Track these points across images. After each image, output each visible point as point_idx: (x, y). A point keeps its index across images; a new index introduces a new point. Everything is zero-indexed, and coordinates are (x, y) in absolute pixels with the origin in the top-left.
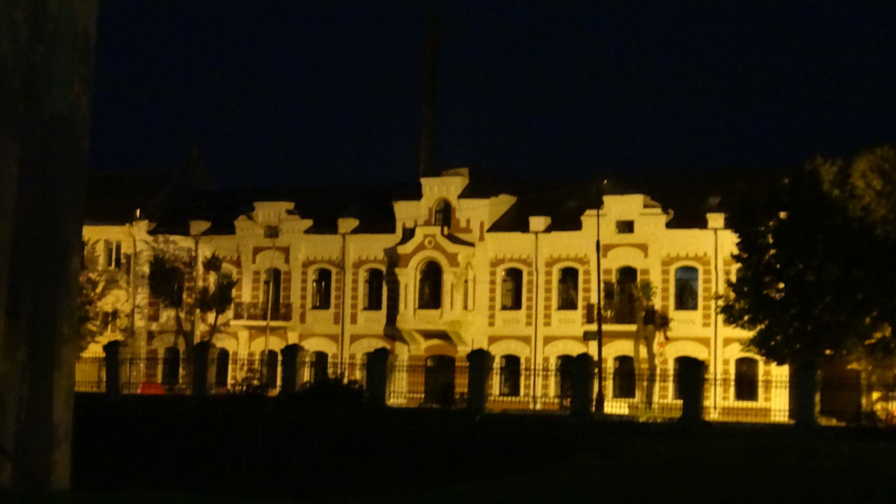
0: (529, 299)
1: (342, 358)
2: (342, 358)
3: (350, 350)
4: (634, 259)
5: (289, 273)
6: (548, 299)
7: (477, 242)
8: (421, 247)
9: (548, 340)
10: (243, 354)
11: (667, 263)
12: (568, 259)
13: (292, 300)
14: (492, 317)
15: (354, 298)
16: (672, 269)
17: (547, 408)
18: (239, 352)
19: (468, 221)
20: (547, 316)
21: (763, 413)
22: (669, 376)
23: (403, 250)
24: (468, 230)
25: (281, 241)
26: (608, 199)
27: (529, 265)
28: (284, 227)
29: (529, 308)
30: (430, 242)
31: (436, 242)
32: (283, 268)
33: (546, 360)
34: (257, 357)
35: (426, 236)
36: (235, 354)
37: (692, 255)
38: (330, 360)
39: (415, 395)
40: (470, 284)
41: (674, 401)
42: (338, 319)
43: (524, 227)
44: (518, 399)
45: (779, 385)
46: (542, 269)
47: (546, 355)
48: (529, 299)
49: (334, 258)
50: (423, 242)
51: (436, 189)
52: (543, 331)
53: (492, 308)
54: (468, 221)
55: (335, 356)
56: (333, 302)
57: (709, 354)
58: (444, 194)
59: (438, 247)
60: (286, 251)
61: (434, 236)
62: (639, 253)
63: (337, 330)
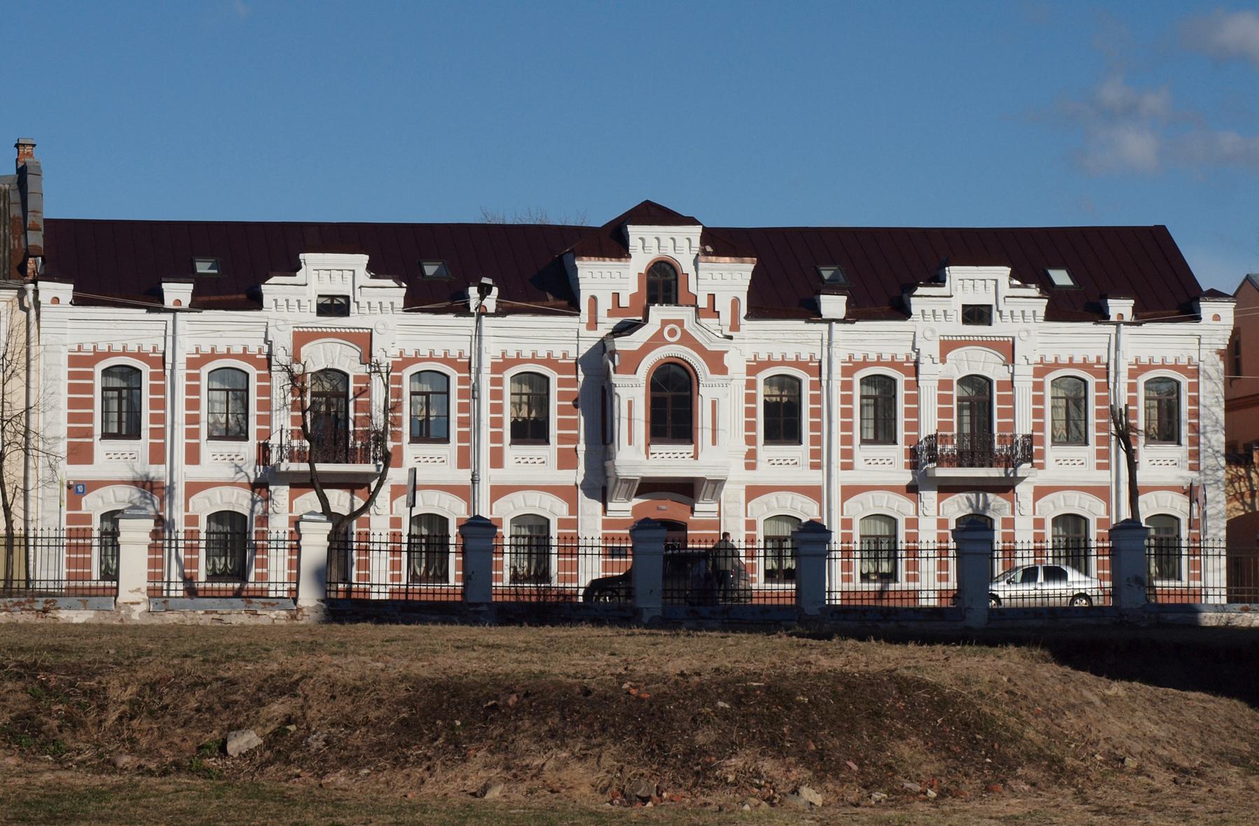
0: (816, 427)
1: (26, 521)
2: (26, 521)
4: (990, 366)
5: (1011, 385)
6: (846, 427)
8: (657, 340)
9: (849, 492)
11: (1042, 370)
12: (783, 363)
14: (751, 455)
16: (1141, 380)
17: (396, 597)
19: (712, 297)
20: (847, 454)
21: (912, 595)
22: (192, 545)
23: (623, 344)
25: (998, 329)
26: (307, 258)
27: (1096, 374)
28: (361, 297)
29: (816, 440)
30: (672, 333)
33: (192, 520)
34: (203, 526)
35: (665, 323)
37: (1078, 359)
38: (554, 531)
41: (768, 586)
42: (464, 460)
43: (1100, 315)
44: (445, 587)
46: (1124, 379)
48: (816, 427)
49: (901, 357)
50: (660, 332)
52: (841, 478)
53: (751, 440)
54: (712, 297)
55: (563, 523)
56: (146, 424)
57: (821, 513)
58: (669, 252)
61: (680, 323)
63: (464, 477)
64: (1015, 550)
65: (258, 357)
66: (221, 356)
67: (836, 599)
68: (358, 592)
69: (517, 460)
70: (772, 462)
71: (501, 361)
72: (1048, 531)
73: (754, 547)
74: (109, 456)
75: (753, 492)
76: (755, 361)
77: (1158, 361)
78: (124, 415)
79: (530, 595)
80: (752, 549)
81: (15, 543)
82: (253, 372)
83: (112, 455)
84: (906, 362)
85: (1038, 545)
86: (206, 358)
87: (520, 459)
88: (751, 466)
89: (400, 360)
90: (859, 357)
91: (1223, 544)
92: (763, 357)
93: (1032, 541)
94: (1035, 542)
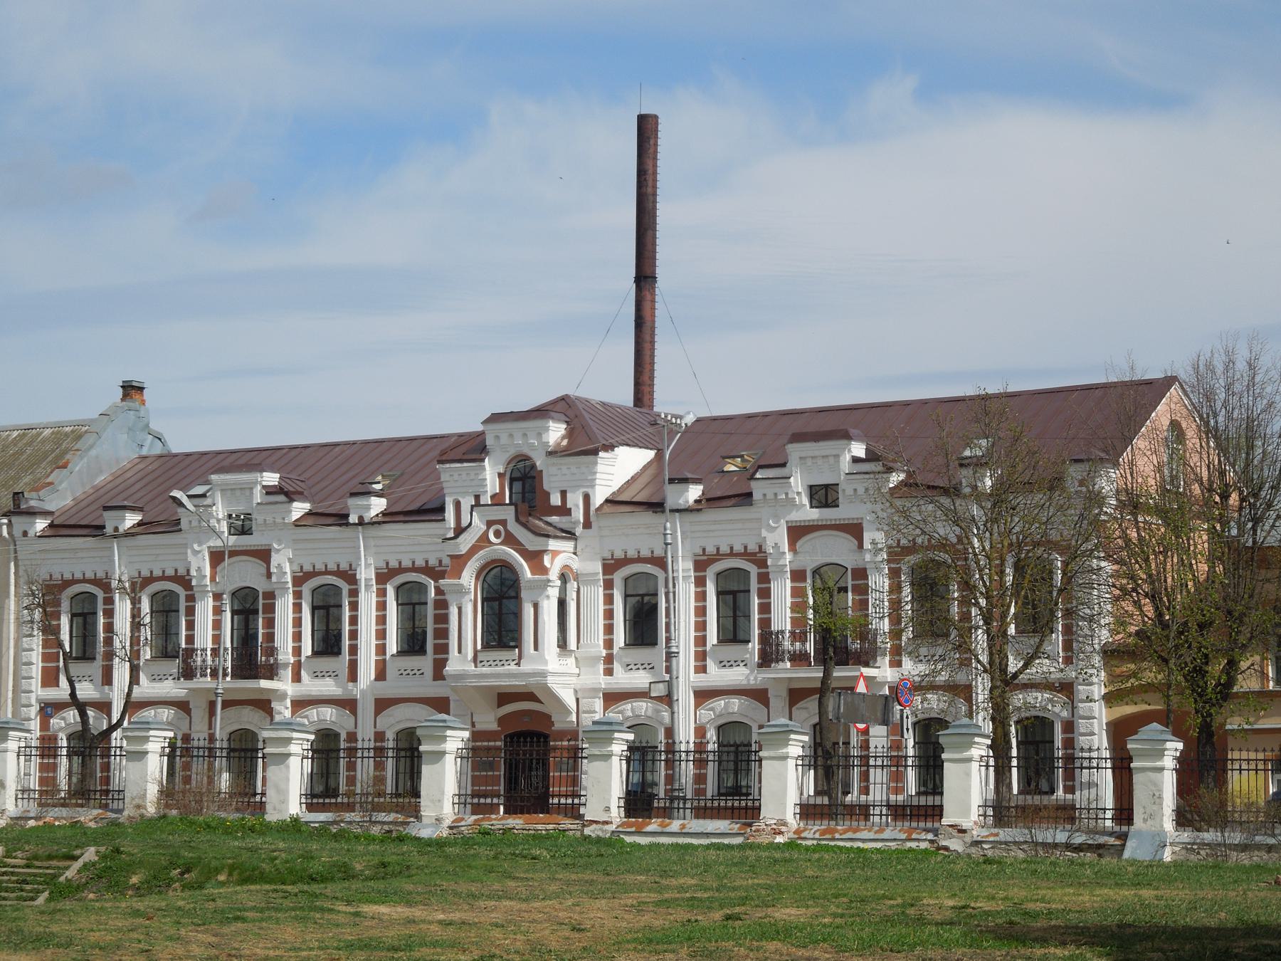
3: (375, 727)
7: (579, 530)
10: (686, 736)
13: (278, 642)
15: (381, 634)
18: (193, 735)
24: (564, 511)
27: (755, 562)
31: (507, 532)
32: (261, 586)
36: (352, 737)
39: (482, 801)
40: (671, 595)
45: (1244, 766)
47: (379, 728)
51: (504, 439)
59: (510, 540)
60: (264, 555)
61: (503, 523)
62: (847, 541)
64: (356, 749)
65: (350, 572)
66: (79, 581)
67: (881, 815)
68: (918, 815)
69: (400, 672)
70: (744, 663)
71: (386, 571)
72: (711, 735)
73: (900, 754)
74: (421, 672)
75: (703, 696)
76: (612, 559)
77: (157, 573)
78: (346, 628)
79: (985, 815)
80: (898, 756)
81: (1056, 765)
82: (101, 595)
83: (418, 673)
84: (759, 553)
85: (378, 744)
86: (308, 576)
87: (402, 671)
88: (702, 669)
89: (301, 574)
90: (711, 550)
91: (1107, 754)
92: (619, 554)
93: (372, 739)
94: (375, 741)
